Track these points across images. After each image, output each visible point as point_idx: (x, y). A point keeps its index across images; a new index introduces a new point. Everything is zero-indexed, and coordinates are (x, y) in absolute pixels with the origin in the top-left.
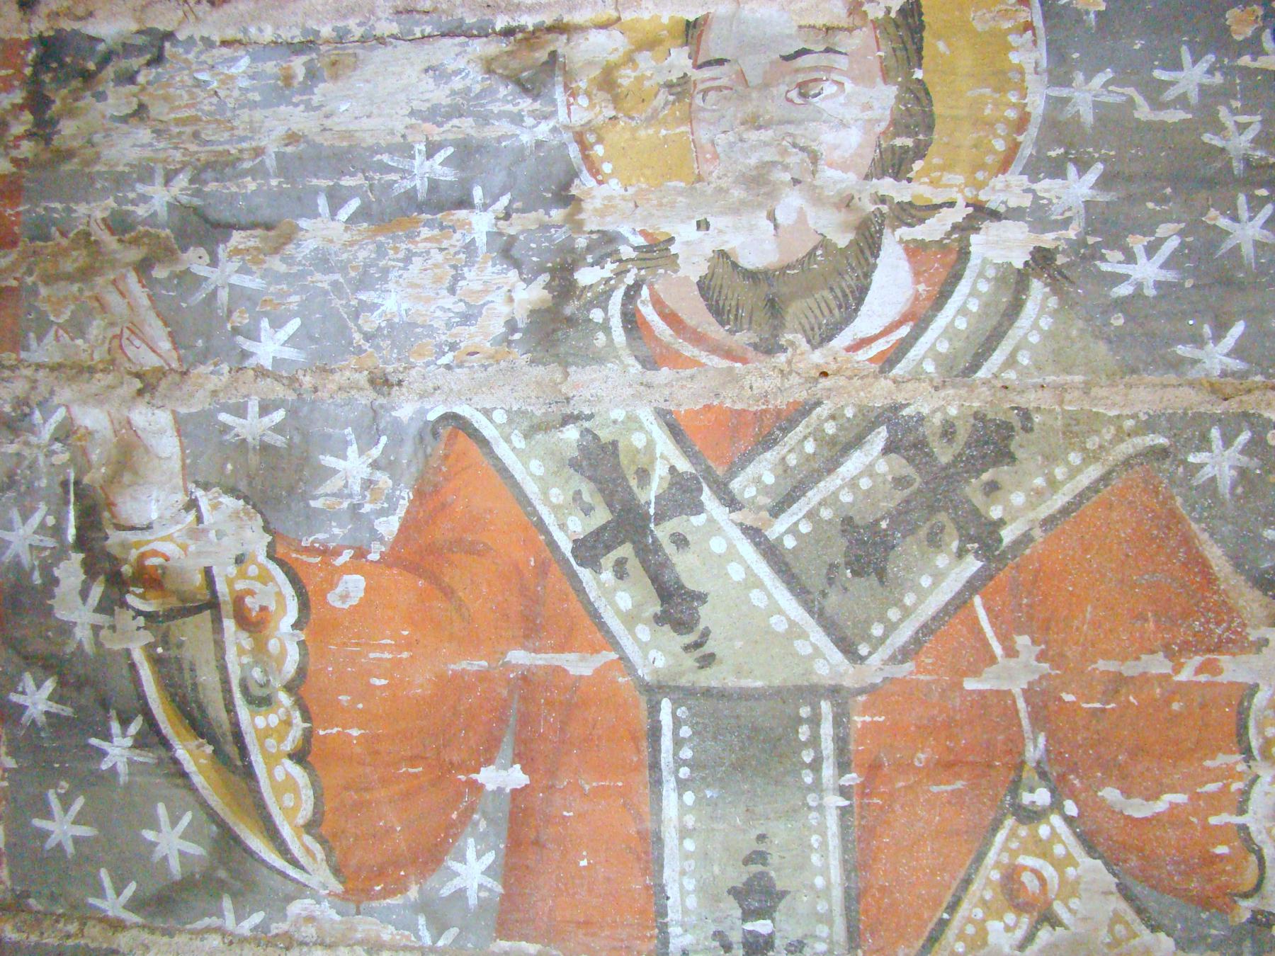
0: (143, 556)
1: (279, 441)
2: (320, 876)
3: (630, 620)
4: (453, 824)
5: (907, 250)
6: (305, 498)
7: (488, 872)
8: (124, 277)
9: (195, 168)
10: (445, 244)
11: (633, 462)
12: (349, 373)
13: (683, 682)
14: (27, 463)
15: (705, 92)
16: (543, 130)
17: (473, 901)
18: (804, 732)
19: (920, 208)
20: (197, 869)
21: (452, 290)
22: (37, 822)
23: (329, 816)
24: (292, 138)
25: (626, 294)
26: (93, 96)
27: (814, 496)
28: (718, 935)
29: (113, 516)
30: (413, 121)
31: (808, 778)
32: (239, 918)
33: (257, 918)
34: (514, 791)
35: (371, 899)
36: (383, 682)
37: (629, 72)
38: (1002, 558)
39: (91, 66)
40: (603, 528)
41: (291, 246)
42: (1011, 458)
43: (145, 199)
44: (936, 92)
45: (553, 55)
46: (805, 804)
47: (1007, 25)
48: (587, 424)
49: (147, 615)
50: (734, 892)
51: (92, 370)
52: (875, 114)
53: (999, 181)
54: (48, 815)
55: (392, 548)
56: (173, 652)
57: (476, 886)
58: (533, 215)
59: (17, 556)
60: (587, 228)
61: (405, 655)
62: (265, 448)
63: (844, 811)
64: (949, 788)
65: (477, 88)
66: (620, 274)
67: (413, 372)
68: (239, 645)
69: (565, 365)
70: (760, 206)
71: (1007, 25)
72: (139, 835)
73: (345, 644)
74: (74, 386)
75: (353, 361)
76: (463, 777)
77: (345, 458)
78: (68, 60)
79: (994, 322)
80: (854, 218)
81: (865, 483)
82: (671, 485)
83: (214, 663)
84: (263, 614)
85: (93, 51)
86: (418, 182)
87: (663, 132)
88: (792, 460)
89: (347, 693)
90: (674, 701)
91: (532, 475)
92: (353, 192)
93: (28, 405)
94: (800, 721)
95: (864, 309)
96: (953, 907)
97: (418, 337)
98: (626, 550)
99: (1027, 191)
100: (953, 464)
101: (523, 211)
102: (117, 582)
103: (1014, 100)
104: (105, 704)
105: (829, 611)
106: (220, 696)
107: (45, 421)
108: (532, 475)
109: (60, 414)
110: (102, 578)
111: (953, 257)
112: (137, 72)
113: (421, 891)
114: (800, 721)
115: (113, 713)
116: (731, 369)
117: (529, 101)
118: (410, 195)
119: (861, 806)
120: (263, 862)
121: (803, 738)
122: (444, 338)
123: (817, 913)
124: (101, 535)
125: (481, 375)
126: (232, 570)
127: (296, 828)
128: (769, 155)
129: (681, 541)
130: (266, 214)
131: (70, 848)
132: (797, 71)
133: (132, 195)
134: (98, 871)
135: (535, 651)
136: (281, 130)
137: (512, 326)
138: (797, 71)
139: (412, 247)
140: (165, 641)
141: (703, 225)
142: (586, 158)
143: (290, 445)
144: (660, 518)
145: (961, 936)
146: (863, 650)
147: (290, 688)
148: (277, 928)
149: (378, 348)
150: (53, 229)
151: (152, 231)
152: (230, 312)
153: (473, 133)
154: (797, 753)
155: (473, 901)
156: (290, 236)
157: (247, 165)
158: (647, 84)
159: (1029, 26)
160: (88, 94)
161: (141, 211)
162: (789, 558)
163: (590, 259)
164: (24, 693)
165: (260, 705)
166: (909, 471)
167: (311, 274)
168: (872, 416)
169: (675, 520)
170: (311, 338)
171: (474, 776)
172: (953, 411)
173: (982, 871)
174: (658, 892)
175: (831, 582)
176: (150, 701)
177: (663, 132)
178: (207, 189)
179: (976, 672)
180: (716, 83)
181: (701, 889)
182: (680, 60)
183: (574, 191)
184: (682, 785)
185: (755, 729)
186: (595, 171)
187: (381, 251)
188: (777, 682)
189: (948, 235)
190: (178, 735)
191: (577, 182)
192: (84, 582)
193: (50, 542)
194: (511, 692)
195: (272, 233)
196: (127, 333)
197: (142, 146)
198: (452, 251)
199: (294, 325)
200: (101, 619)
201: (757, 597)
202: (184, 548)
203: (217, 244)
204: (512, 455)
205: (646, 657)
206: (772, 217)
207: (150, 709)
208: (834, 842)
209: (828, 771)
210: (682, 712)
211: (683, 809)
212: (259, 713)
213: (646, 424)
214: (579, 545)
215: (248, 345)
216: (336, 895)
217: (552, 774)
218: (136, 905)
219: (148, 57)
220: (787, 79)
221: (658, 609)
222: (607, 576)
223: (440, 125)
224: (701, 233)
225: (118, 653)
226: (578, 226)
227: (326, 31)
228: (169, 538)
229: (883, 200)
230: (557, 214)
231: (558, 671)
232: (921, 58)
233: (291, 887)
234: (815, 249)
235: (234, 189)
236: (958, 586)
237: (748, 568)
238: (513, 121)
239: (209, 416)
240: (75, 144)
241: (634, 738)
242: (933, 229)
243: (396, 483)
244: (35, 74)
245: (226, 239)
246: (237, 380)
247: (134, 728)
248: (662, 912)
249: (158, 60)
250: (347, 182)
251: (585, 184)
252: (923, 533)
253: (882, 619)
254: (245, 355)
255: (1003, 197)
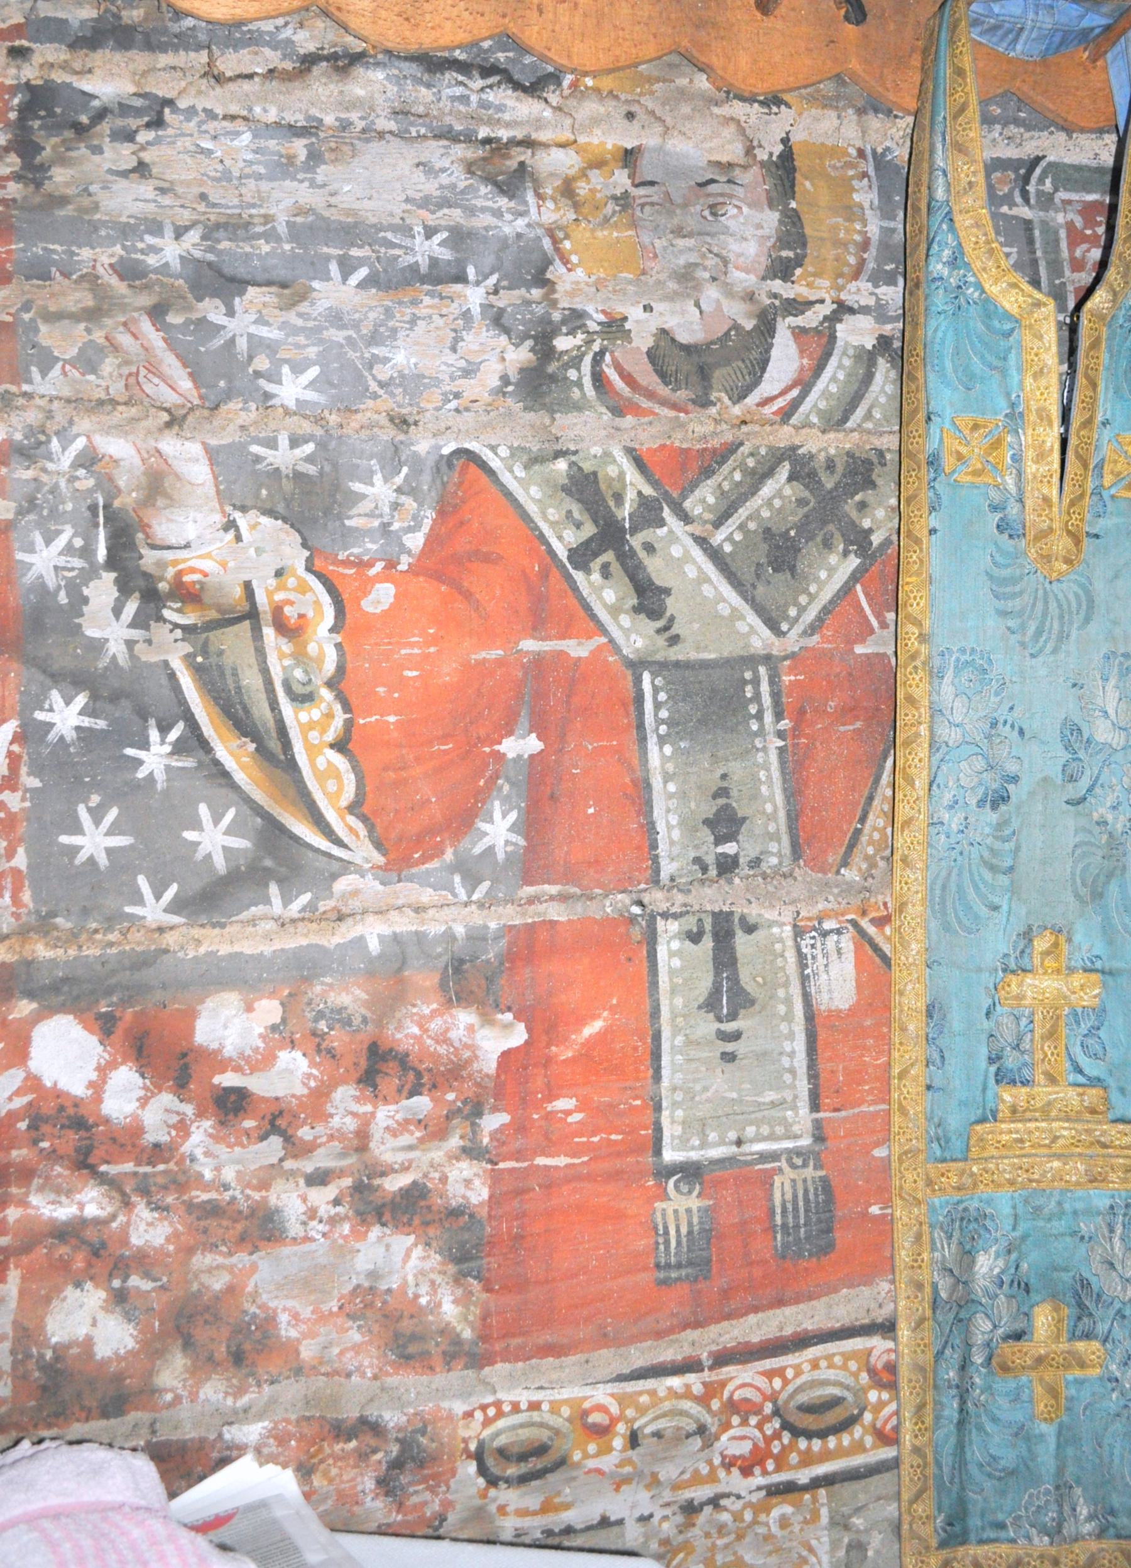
0: (180, 574)
1: (311, 470)
2: (363, 852)
3: (615, 611)
4: (480, 791)
5: (793, 333)
6: (340, 517)
7: (512, 829)
8: (135, 321)
9: (206, 227)
10: (444, 311)
11: (610, 486)
12: (372, 411)
13: (659, 657)
14: (46, 488)
15: (643, 206)
16: (520, 223)
17: (501, 856)
18: (749, 692)
19: (801, 303)
20: (242, 862)
21: (454, 349)
22: (64, 839)
23: (370, 796)
24: (300, 211)
25: (594, 359)
26: (87, 147)
27: (743, 513)
28: (697, 860)
29: (148, 536)
30: (409, 207)
31: (755, 727)
32: (287, 901)
33: (305, 898)
34: (532, 756)
35: (412, 867)
36: (415, 673)
37: (583, 184)
38: (873, 557)
39: (84, 119)
40: (591, 540)
41: (306, 303)
42: (872, 485)
43: (154, 250)
44: (805, 218)
45: (522, 164)
46: (754, 747)
47: (851, 173)
48: (573, 458)
49: (184, 628)
50: (707, 822)
51: (114, 403)
52: (766, 231)
53: (853, 286)
54: (78, 830)
55: (419, 560)
56: (213, 660)
57: (502, 843)
58: (516, 292)
59: (41, 576)
60: (560, 306)
61: (432, 650)
62: (298, 476)
63: (781, 750)
64: (851, 728)
65: (462, 185)
66: (589, 343)
67: (428, 414)
68: (279, 649)
69: (552, 412)
70: (688, 296)
71: (851, 173)
72: (179, 836)
73: (377, 644)
74: (93, 418)
75: (370, 403)
76: (487, 750)
77: (372, 485)
78: (58, 110)
79: (856, 386)
80: (755, 309)
81: (777, 503)
82: (640, 505)
83: (256, 668)
84: (302, 622)
85: (85, 107)
86: (419, 258)
87: (615, 234)
88: (726, 486)
89: (384, 685)
90: (652, 673)
91: (533, 499)
92: (361, 262)
93: (43, 432)
94: (745, 682)
95: (766, 375)
96: (863, 819)
97: (426, 386)
98: (609, 556)
99: (872, 294)
100: (836, 488)
101: (509, 288)
102: (152, 600)
103: (858, 228)
104: (143, 715)
105: (758, 599)
106: (263, 696)
107: (64, 449)
108: (533, 499)
109: (80, 443)
110: (137, 594)
111: (825, 340)
112: (136, 132)
113: (455, 853)
114: (745, 682)
115: (152, 722)
116: (677, 418)
117: (506, 200)
118: (414, 268)
119: (794, 745)
120: (309, 846)
121: (749, 695)
122: (448, 388)
123: (768, 833)
124: (136, 555)
125: (485, 418)
126: (272, 582)
127: (339, 810)
128: (693, 258)
129: (649, 548)
130: (282, 273)
131: (103, 861)
132: (709, 195)
133: (140, 245)
134: (135, 879)
135: (542, 640)
136: (288, 202)
137: (505, 380)
138: (709, 195)
139: (417, 312)
140: (205, 651)
141: (648, 308)
142: (557, 250)
143: (321, 473)
144: (634, 530)
145: (871, 842)
146: (784, 627)
147: (330, 684)
148: (324, 906)
149: (392, 395)
150: (53, 269)
151: (165, 280)
152: (251, 358)
153: (462, 221)
154: (746, 707)
155: (501, 856)
156: (304, 295)
157: (259, 229)
158: (598, 195)
159: (865, 175)
160: (82, 145)
161: (152, 261)
162: (728, 560)
163: (564, 330)
164: (51, 710)
165: (303, 702)
166: (806, 494)
167: (327, 329)
168: (778, 454)
169: (645, 532)
170: (332, 385)
171: (496, 747)
172: (832, 451)
173: (879, 790)
174: (651, 828)
175: (758, 576)
176: (192, 706)
177: (615, 234)
178: (221, 246)
179: (862, 641)
180: (649, 200)
181: (682, 823)
182: (621, 179)
183: (548, 275)
184: (662, 740)
185: (713, 690)
186: (565, 261)
187: (388, 313)
188: (726, 654)
189: (821, 323)
190: (220, 737)
191: (551, 268)
192: (117, 599)
193: (77, 563)
194: (526, 674)
195: (286, 291)
196: (143, 372)
197: (145, 201)
198: (451, 317)
199: (313, 372)
200: (136, 634)
201: (707, 590)
202: (224, 565)
203: (233, 297)
204: (515, 483)
205: (628, 639)
206: (697, 305)
207: (193, 715)
208: (776, 774)
209: (768, 717)
210: (659, 681)
211: (664, 759)
212: (302, 709)
213: (618, 459)
214: (573, 553)
215: (271, 388)
216: (379, 867)
217: (562, 738)
218: (175, 907)
219: (146, 119)
220: (701, 201)
221: (635, 601)
222: (596, 577)
223: (433, 212)
224: (647, 314)
225: (156, 664)
226: (554, 304)
227: (329, 120)
228: (208, 556)
229: (775, 296)
230: (536, 293)
231: (562, 654)
232: (794, 193)
233: (336, 866)
234: (730, 330)
235: (248, 249)
236: (845, 578)
237: (699, 568)
238: (494, 215)
239: (241, 448)
240: (70, 191)
241: (624, 705)
242: (811, 319)
243: (421, 505)
244: (22, 119)
245: (242, 293)
246: (267, 416)
247: (174, 735)
248: (654, 846)
249: (158, 123)
250: (355, 252)
251: (558, 270)
252: (819, 539)
253: (796, 604)
254: (267, 396)
255: (856, 298)
